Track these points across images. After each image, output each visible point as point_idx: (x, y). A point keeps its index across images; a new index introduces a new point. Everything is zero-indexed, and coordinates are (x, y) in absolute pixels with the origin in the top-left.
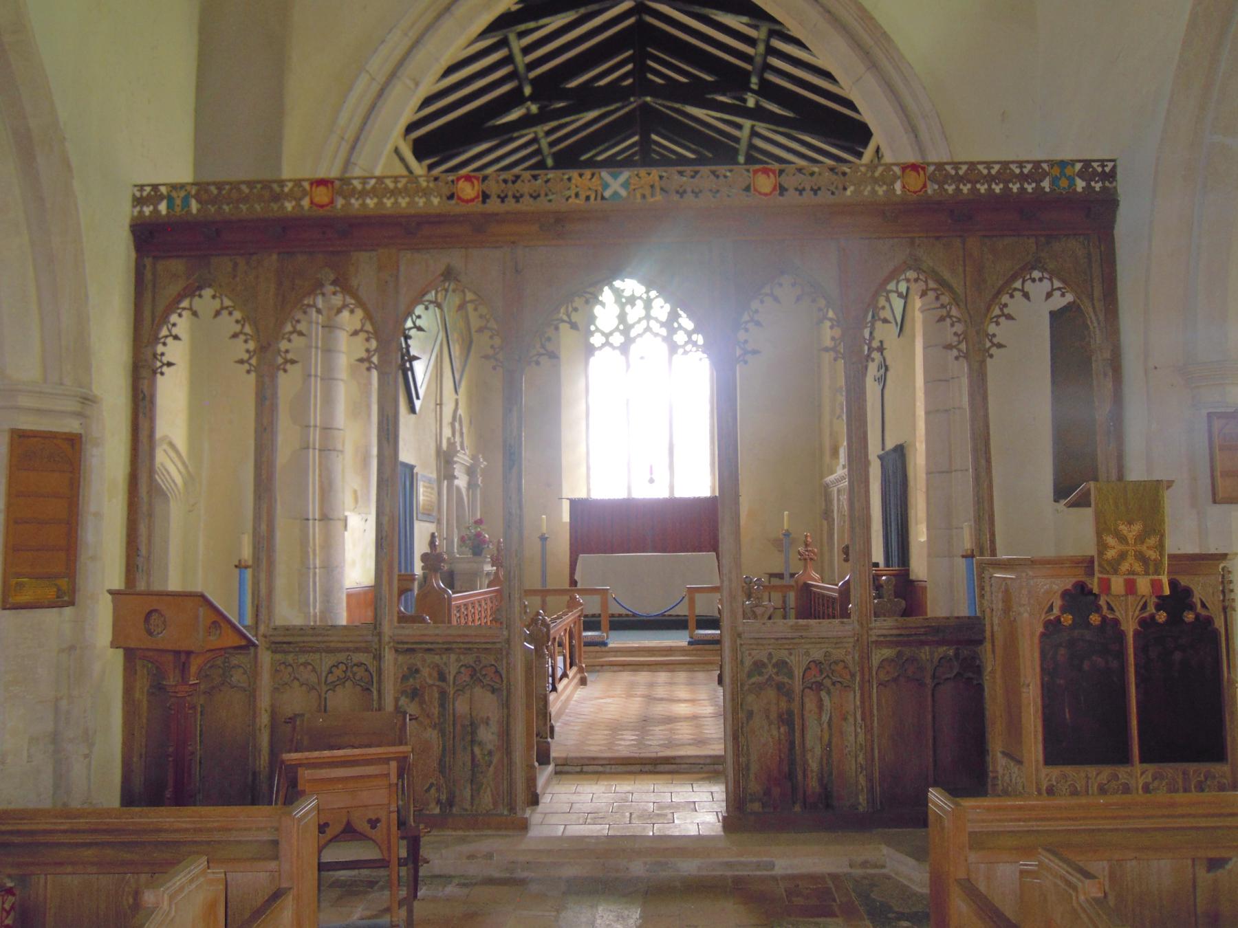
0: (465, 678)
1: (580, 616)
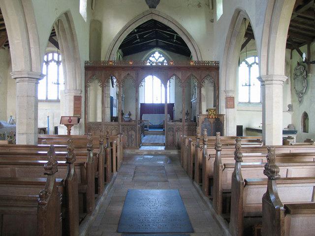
0: (130, 129)
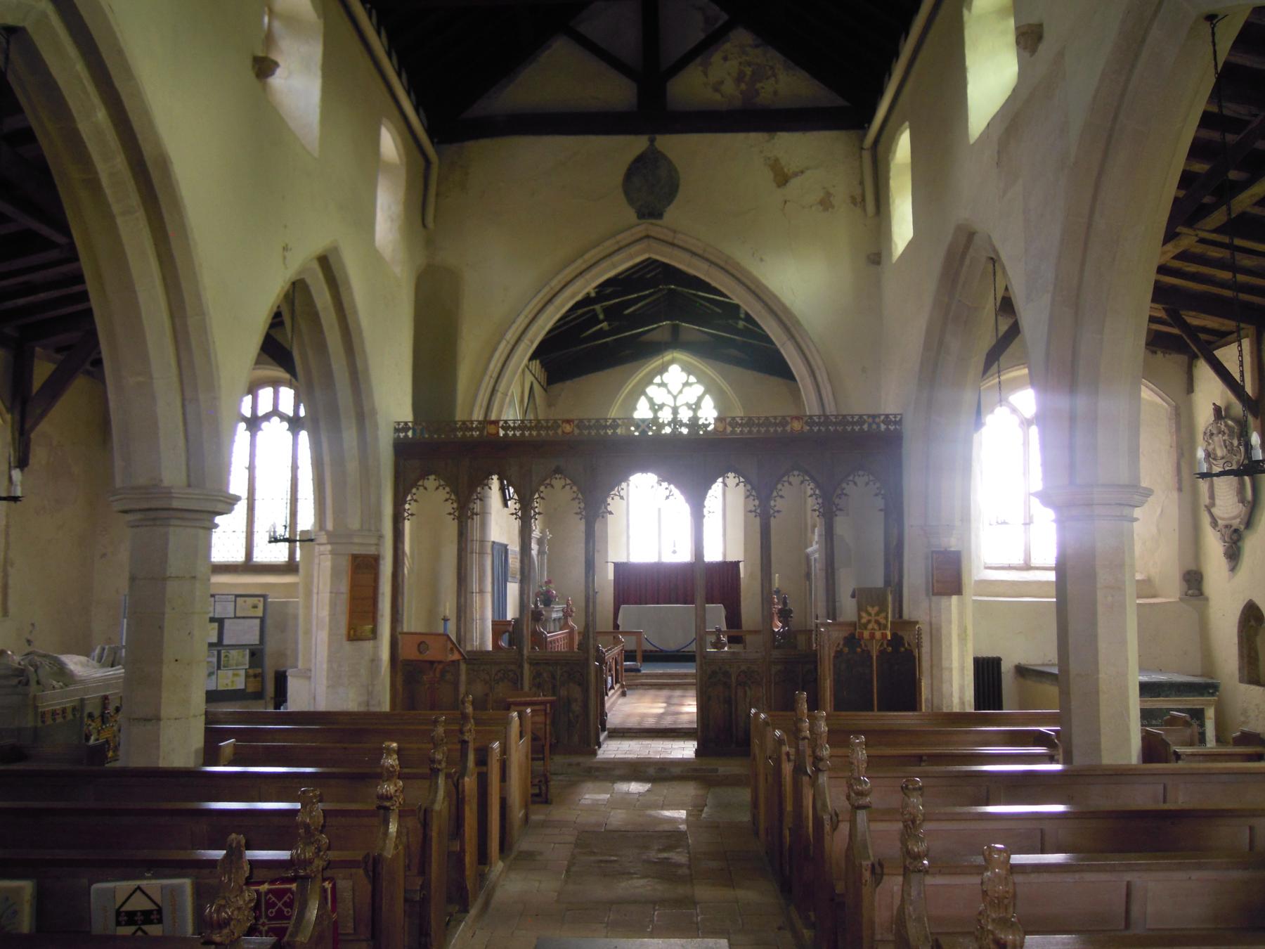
1: (622, 650)
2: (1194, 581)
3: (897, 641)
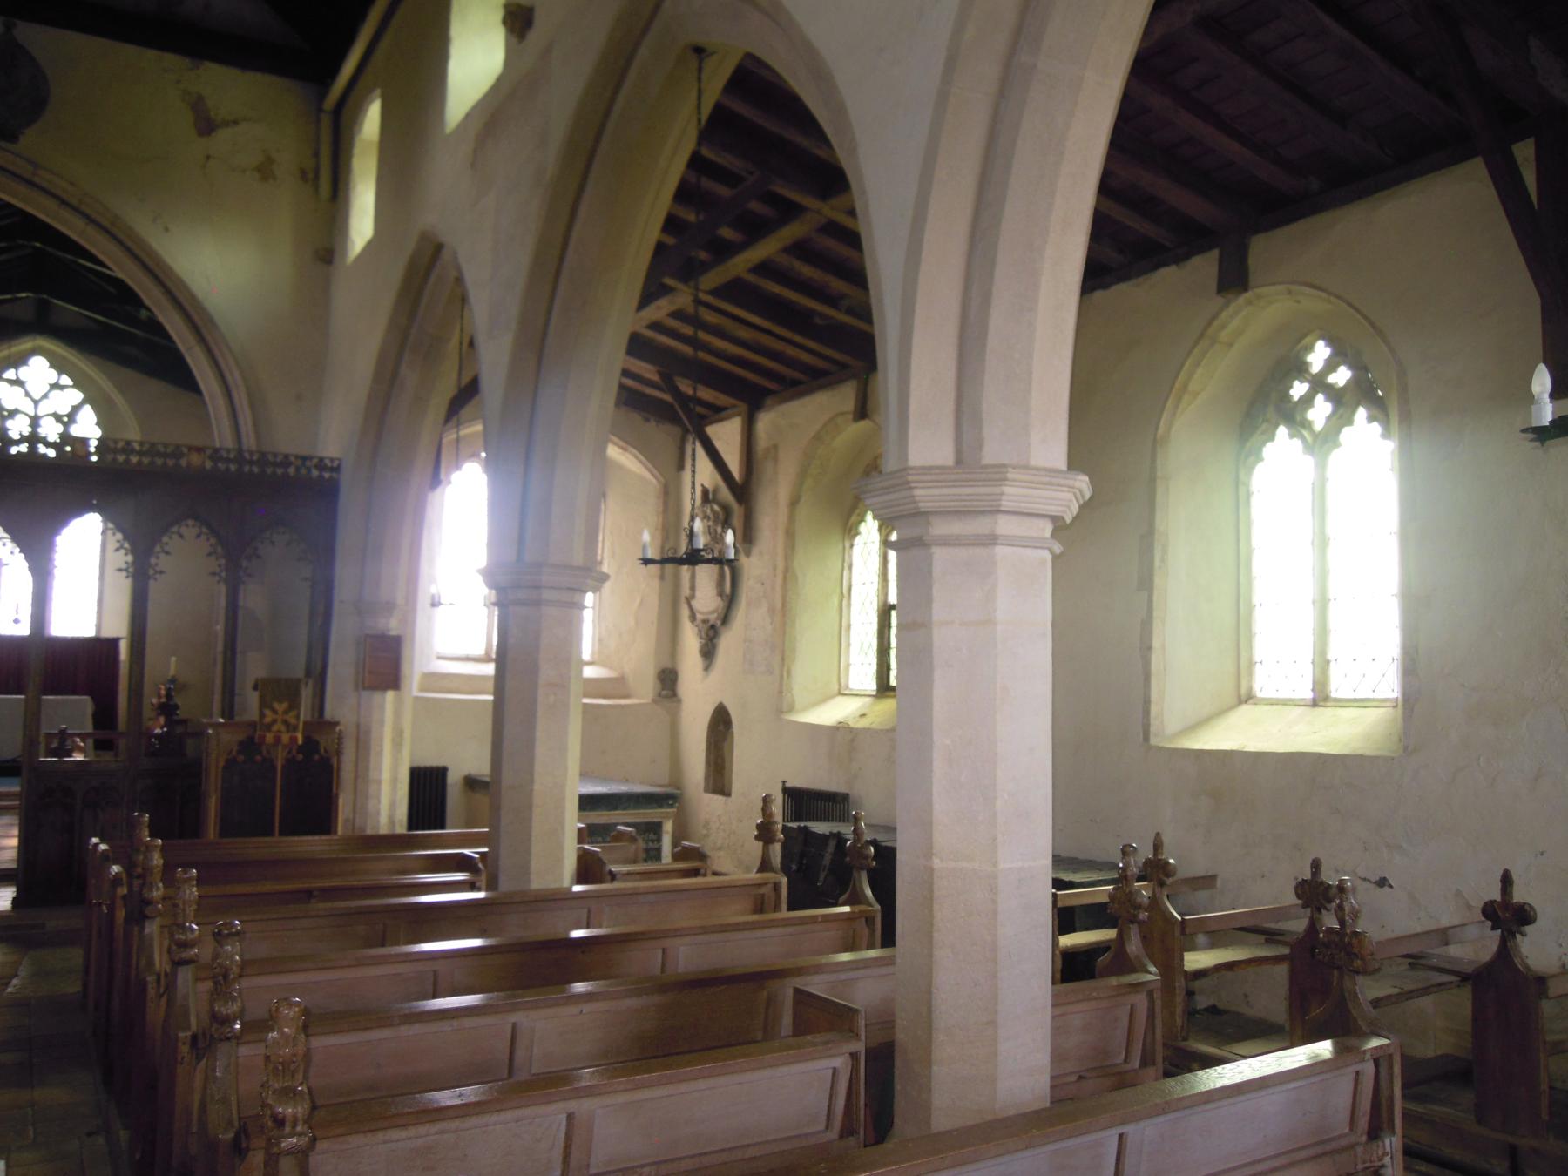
2: (668, 680)
3: (310, 745)
